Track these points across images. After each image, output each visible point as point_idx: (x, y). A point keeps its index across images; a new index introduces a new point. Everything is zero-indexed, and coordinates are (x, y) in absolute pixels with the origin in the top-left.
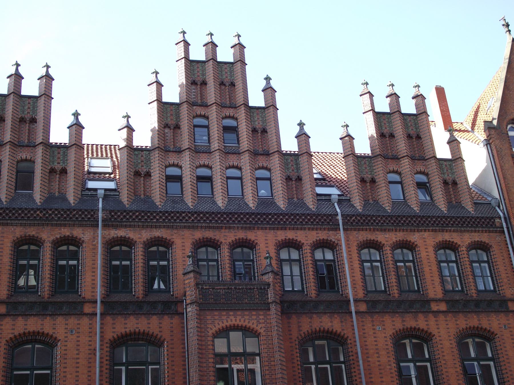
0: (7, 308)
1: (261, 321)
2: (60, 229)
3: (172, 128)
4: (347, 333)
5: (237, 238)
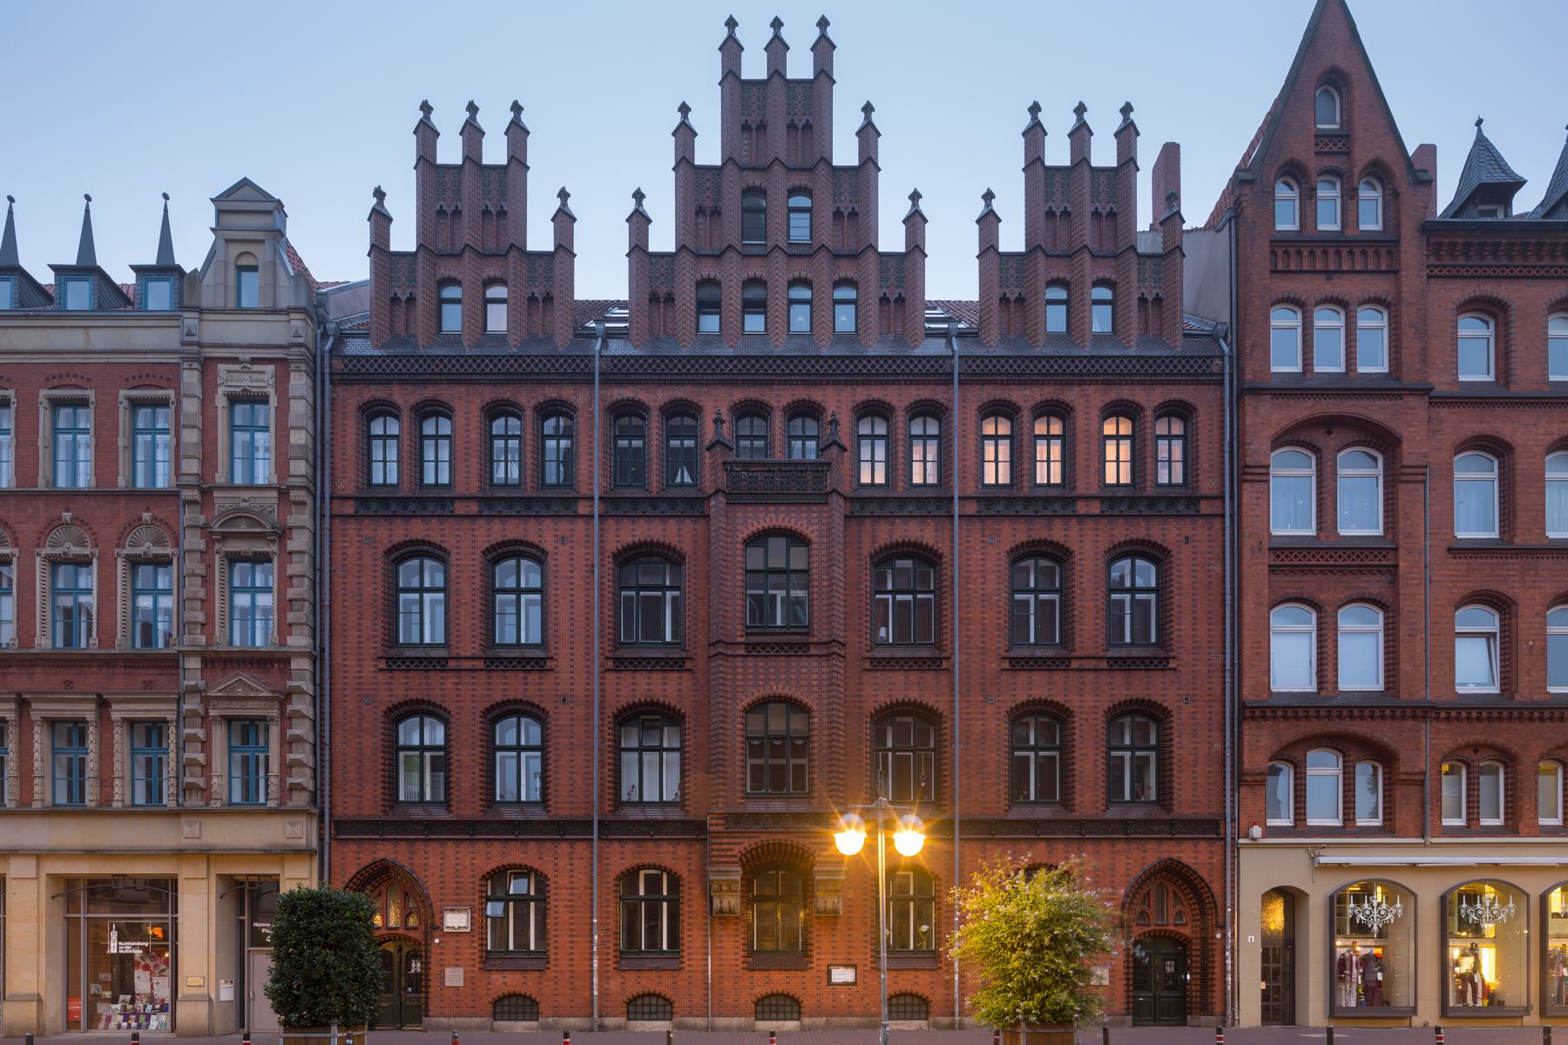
4: (943, 548)
5: (795, 398)
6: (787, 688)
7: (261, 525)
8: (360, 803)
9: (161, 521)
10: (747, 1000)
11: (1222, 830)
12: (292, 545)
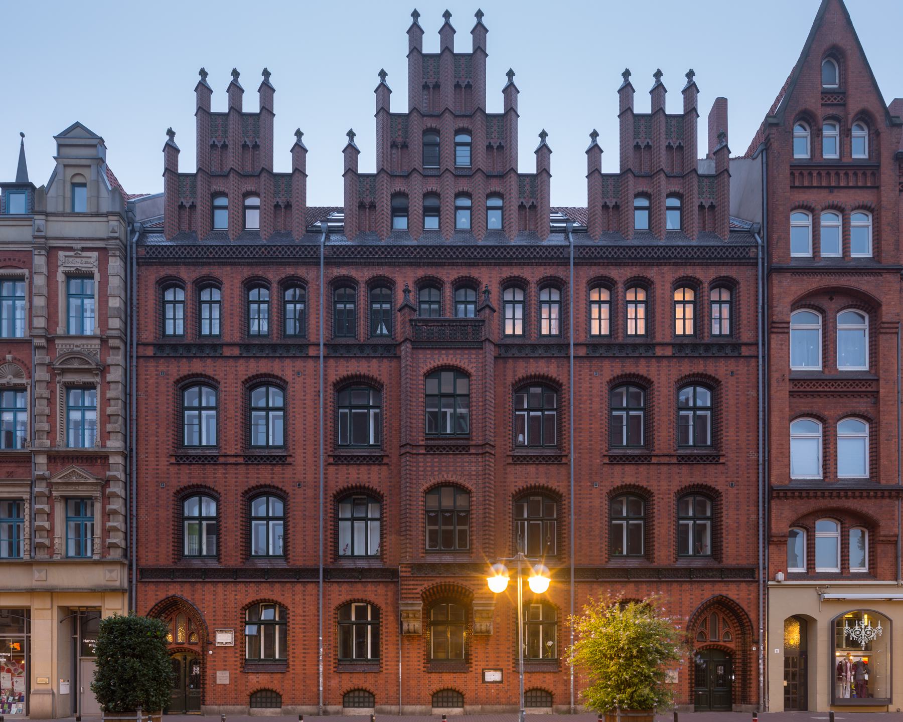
2: (285, 269)
3: (399, 146)
4: (562, 379)
7: (89, 363)
8: (158, 556)
9: (19, 360)
10: (426, 694)
11: (757, 575)
12: (110, 377)
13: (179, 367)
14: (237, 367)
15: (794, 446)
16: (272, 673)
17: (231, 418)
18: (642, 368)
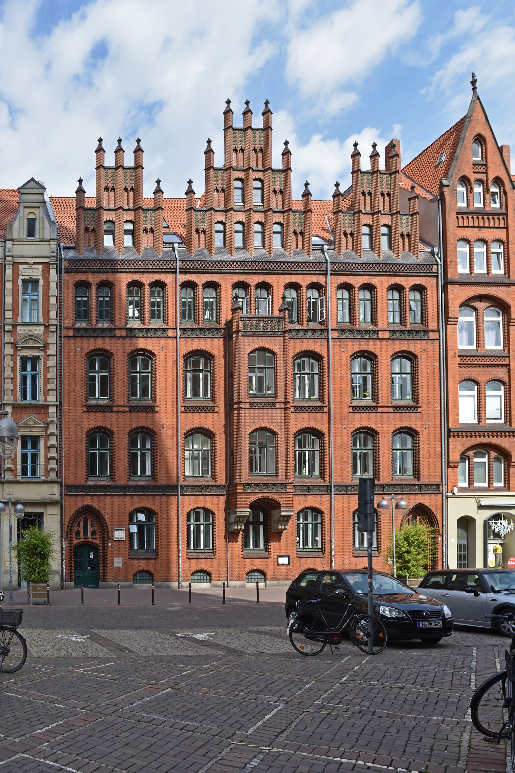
0: (126, 332)
1: (277, 344)
6: (267, 423)
8: (76, 477)
10: (243, 573)
11: (441, 489)
12: (49, 352)
13: (88, 344)
14: (124, 344)
15: (461, 400)
16: (148, 559)
17: (121, 379)
18: (370, 346)
